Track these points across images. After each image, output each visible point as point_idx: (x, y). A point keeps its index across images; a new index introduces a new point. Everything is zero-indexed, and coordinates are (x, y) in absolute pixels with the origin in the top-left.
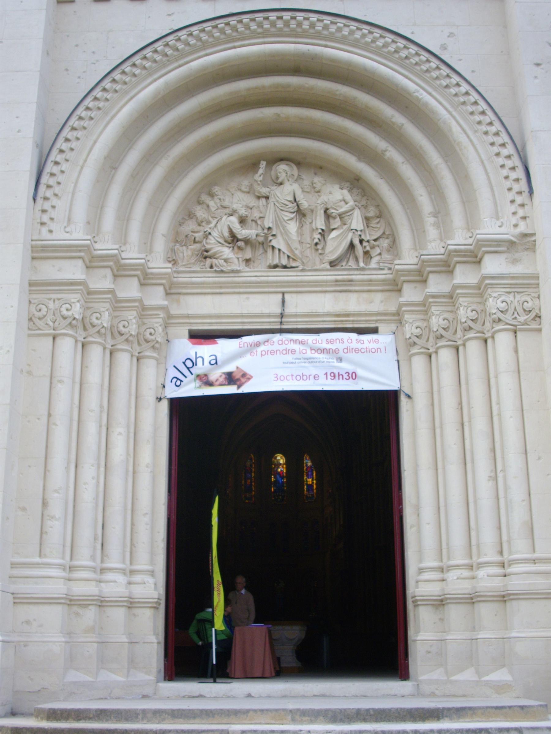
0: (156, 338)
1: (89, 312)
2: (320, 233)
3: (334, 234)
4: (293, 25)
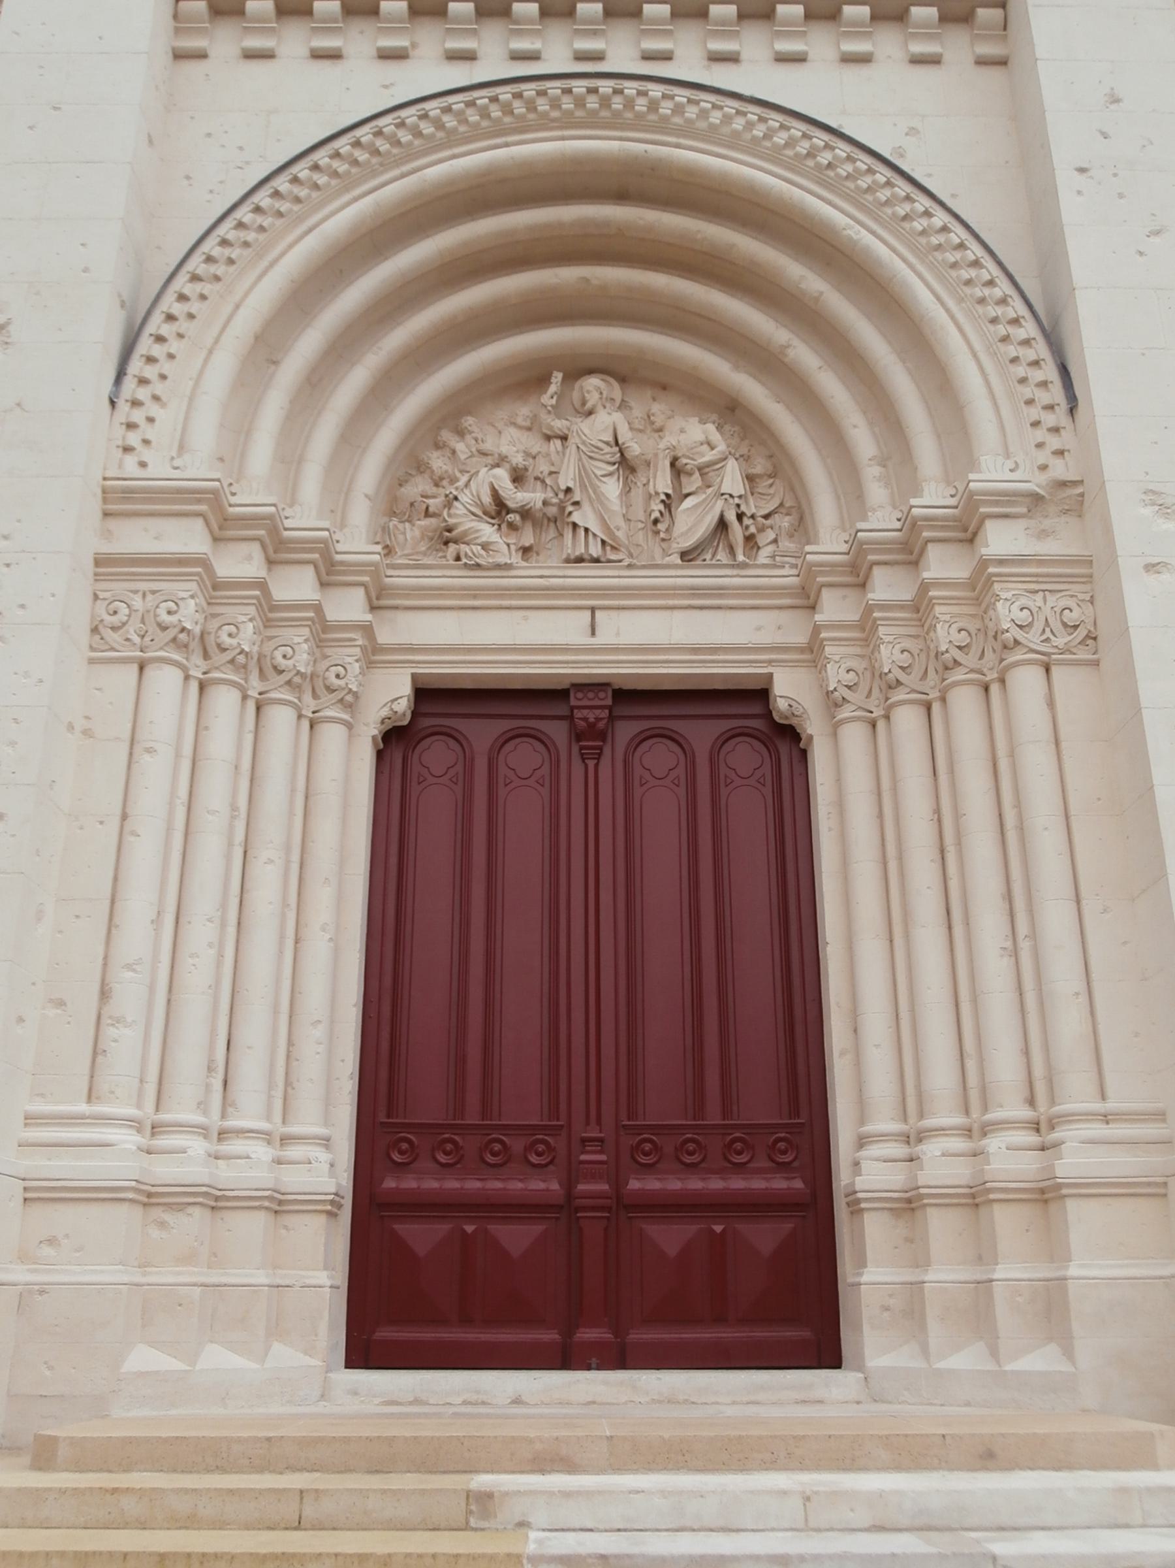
0: (347, 684)
1: (213, 625)
2: (663, 501)
3: (689, 502)
4: (617, 103)
